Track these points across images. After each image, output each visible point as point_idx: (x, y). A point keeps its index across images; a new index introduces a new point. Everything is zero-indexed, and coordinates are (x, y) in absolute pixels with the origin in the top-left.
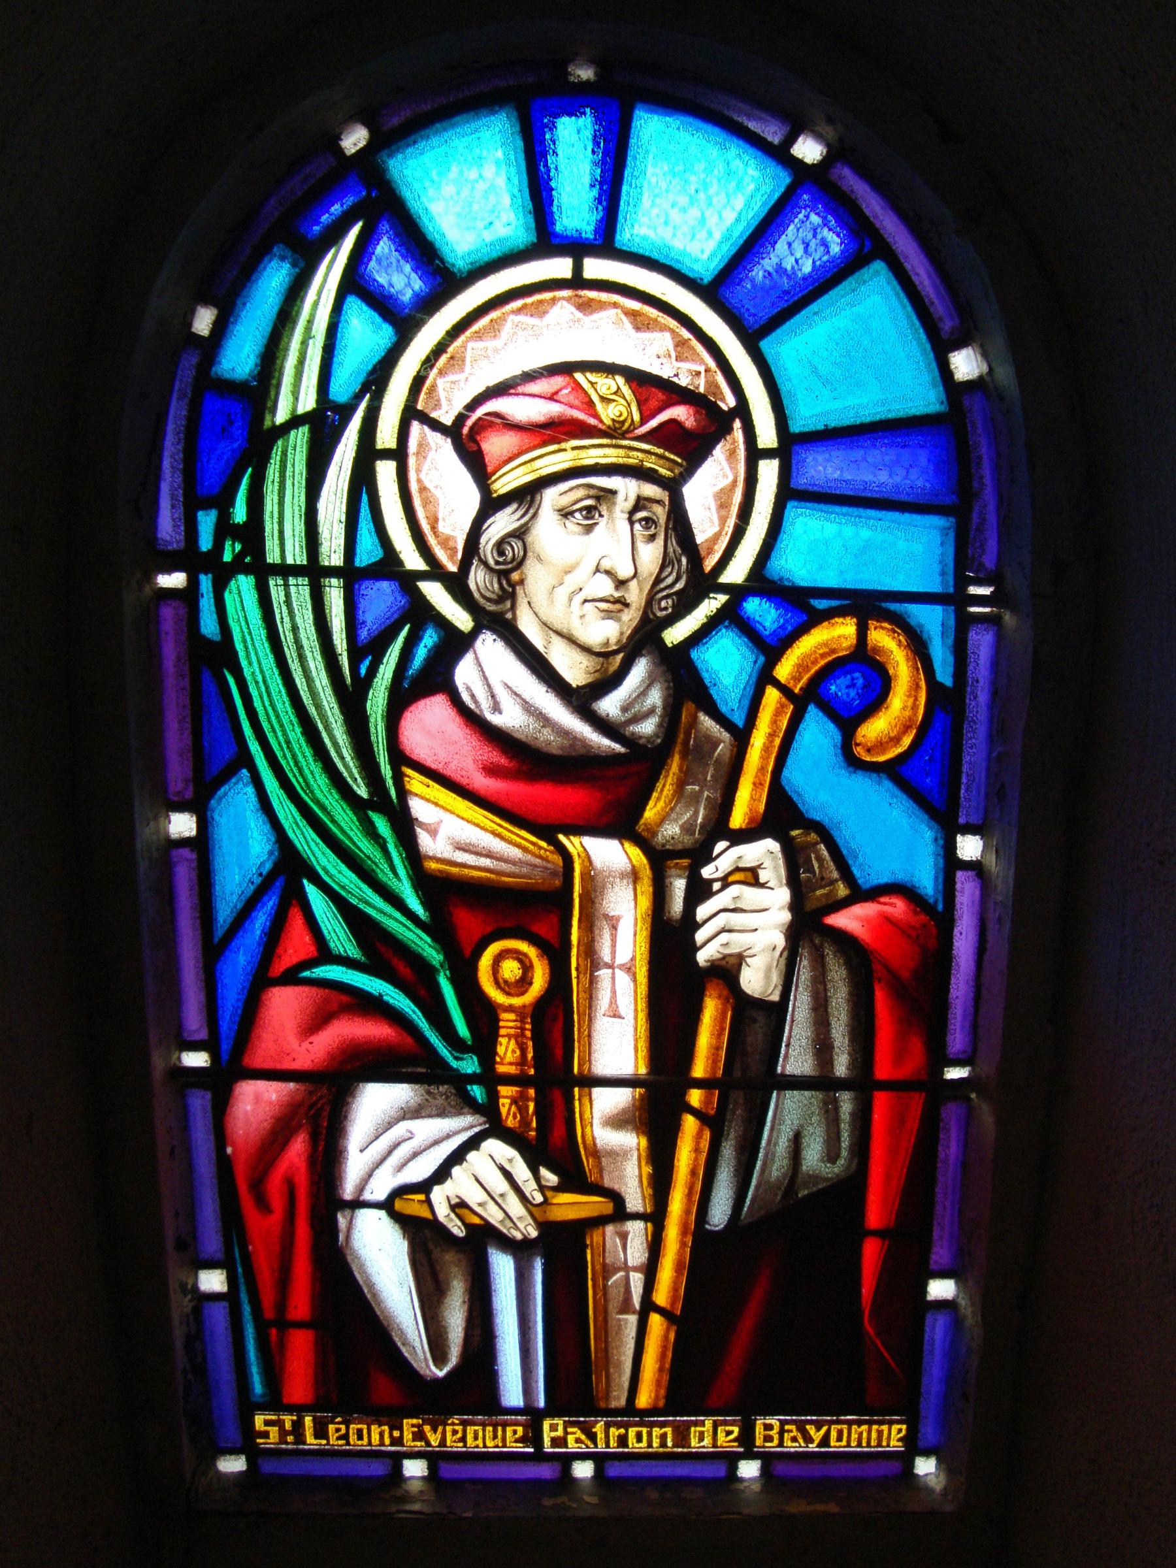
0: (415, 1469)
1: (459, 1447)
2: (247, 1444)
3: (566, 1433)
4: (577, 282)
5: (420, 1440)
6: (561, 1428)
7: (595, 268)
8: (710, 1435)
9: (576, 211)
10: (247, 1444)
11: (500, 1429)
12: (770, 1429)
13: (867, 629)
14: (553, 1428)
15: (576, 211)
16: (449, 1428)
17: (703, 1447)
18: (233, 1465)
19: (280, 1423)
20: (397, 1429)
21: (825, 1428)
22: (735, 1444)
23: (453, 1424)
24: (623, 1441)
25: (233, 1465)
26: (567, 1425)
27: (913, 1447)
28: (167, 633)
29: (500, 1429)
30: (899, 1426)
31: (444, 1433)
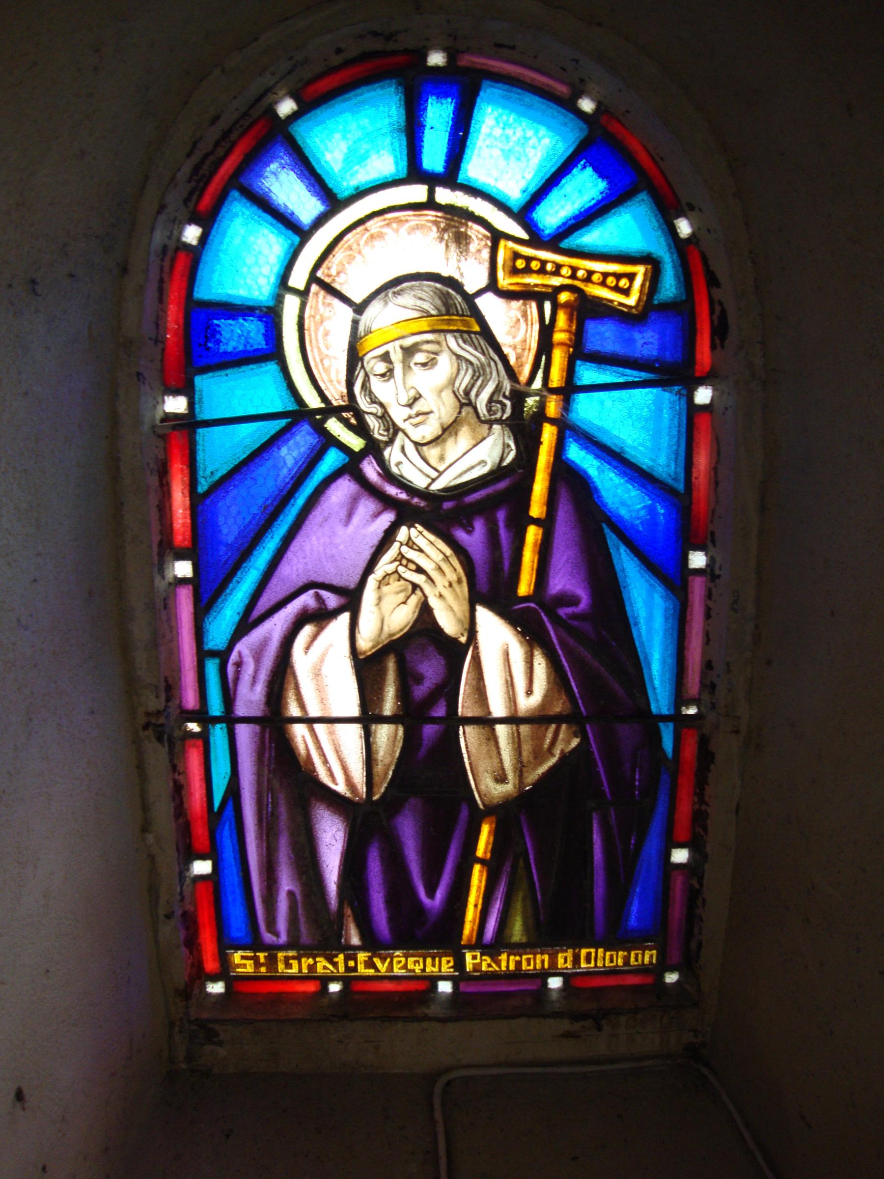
0: (555, 983)
1: (403, 972)
2: (224, 972)
3: (482, 960)
4: (431, 204)
5: (369, 968)
6: (479, 957)
7: (443, 195)
8: (541, 960)
9: (434, 157)
10: (224, 972)
11: (437, 959)
12: (564, 960)
13: (266, 336)
14: (474, 957)
15: (434, 157)
16: (395, 960)
17: (566, 968)
18: (216, 988)
19: (256, 959)
20: (351, 959)
21: (388, 960)
22: (452, 970)
23: (398, 956)
24: (312, 968)
25: (216, 988)
26: (482, 955)
27: (663, 966)
28: (398, 464)
29: (437, 959)
30: (448, 959)
31: (391, 963)
